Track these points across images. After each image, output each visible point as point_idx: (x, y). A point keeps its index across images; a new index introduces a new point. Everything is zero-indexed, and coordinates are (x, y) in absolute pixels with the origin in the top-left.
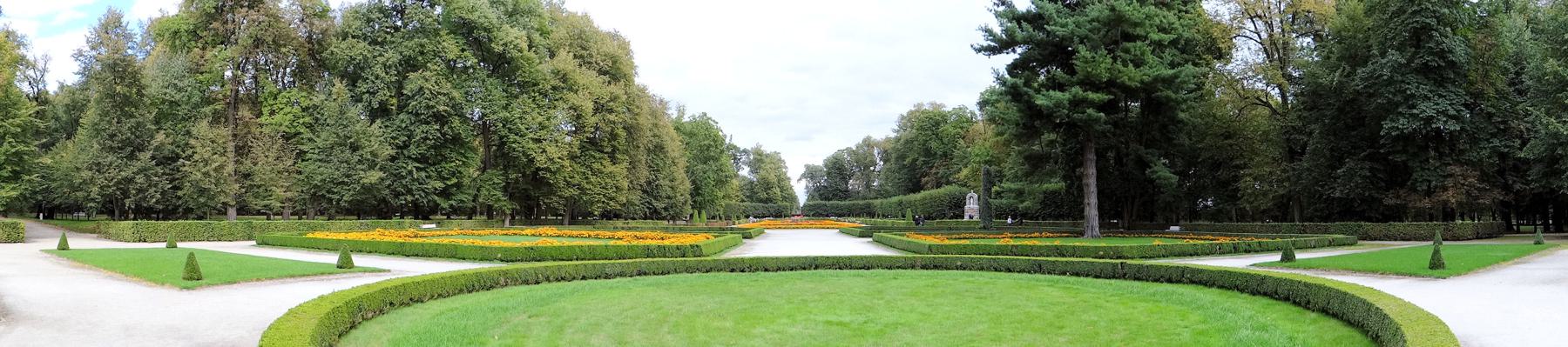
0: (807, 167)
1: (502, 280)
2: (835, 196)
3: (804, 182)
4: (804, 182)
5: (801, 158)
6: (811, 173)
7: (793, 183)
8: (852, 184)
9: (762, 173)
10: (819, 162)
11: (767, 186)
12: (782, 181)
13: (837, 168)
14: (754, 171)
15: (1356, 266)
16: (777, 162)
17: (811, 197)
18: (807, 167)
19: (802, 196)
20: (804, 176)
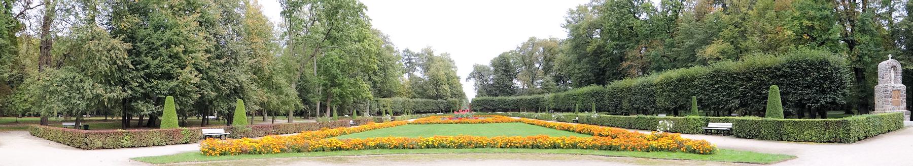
0: (476, 67)
1: (625, 104)
2: (503, 92)
3: (472, 82)
4: (472, 82)
5: (469, 54)
6: (479, 73)
7: (463, 81)
8: (518, 84)
9: (432, 70)
10: (486, 61)
11: (436, 82)
12: (452, 79)
13: (504, 66)
14: (426, 69)
15: (426, 109)
16: (447, 63)
17: (480, 93)
18: (476, 67)
19: (470, 92)
20: (472, 75)
